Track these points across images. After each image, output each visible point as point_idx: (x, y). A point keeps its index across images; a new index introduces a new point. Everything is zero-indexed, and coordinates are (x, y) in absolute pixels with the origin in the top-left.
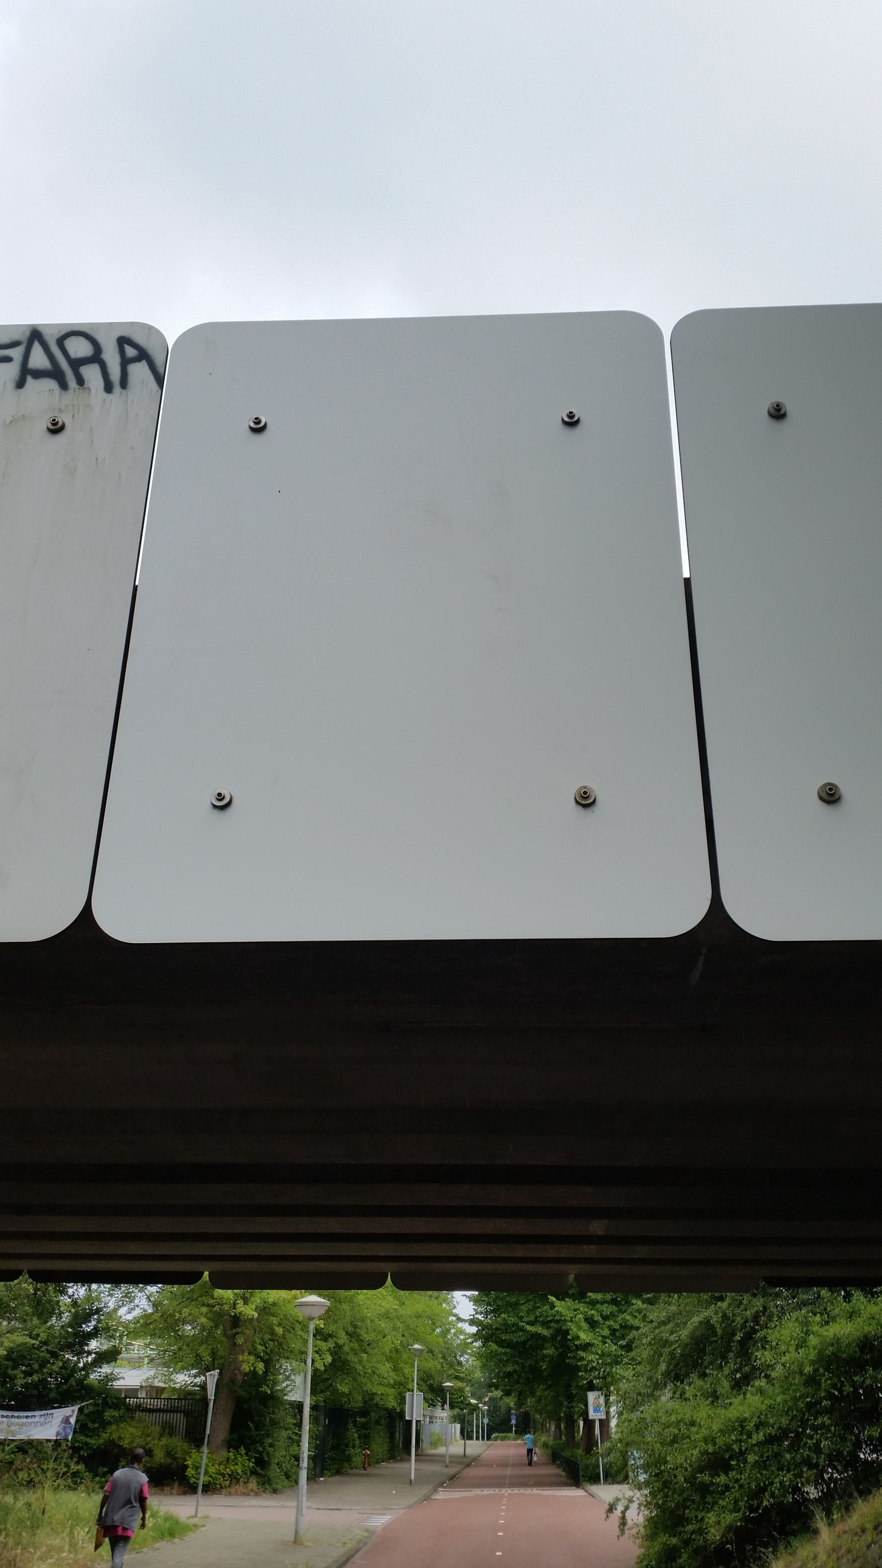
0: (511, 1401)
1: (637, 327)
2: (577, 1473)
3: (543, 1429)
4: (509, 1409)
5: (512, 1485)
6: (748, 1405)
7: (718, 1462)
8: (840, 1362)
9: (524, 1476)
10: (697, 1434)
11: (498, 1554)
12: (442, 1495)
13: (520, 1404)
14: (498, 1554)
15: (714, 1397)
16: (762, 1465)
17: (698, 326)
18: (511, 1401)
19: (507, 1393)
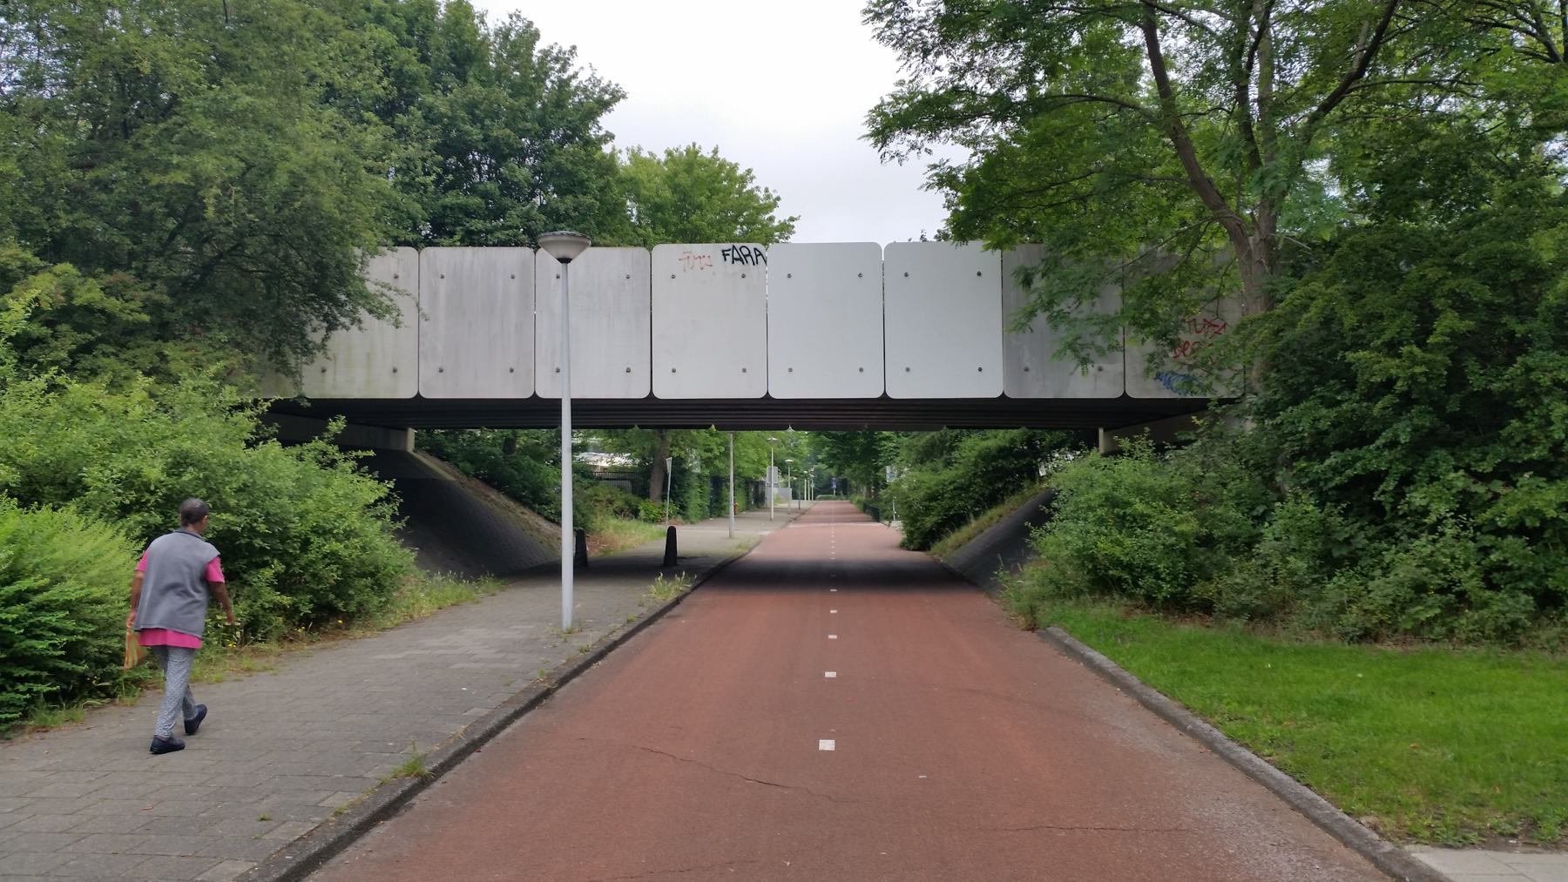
0: (833, 472)
1: (876, 246)
2: (877, 515)
3: (858, 491)
4: (830, 478)
5: (836, 521)
6: (947, 475)
7: (933, 497)
8: (986, 457)
9: (843, 517)
10: (924, 486)
11: (828, 674)
12: (791, 526)
13: (839, 473)
14: (828, 674)
15: (935, 470)
16: (952, 498)
17: (893, 247)
18: (833, 472)
19: (831, 466)
